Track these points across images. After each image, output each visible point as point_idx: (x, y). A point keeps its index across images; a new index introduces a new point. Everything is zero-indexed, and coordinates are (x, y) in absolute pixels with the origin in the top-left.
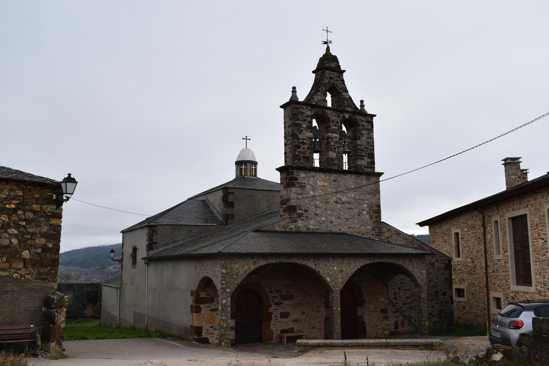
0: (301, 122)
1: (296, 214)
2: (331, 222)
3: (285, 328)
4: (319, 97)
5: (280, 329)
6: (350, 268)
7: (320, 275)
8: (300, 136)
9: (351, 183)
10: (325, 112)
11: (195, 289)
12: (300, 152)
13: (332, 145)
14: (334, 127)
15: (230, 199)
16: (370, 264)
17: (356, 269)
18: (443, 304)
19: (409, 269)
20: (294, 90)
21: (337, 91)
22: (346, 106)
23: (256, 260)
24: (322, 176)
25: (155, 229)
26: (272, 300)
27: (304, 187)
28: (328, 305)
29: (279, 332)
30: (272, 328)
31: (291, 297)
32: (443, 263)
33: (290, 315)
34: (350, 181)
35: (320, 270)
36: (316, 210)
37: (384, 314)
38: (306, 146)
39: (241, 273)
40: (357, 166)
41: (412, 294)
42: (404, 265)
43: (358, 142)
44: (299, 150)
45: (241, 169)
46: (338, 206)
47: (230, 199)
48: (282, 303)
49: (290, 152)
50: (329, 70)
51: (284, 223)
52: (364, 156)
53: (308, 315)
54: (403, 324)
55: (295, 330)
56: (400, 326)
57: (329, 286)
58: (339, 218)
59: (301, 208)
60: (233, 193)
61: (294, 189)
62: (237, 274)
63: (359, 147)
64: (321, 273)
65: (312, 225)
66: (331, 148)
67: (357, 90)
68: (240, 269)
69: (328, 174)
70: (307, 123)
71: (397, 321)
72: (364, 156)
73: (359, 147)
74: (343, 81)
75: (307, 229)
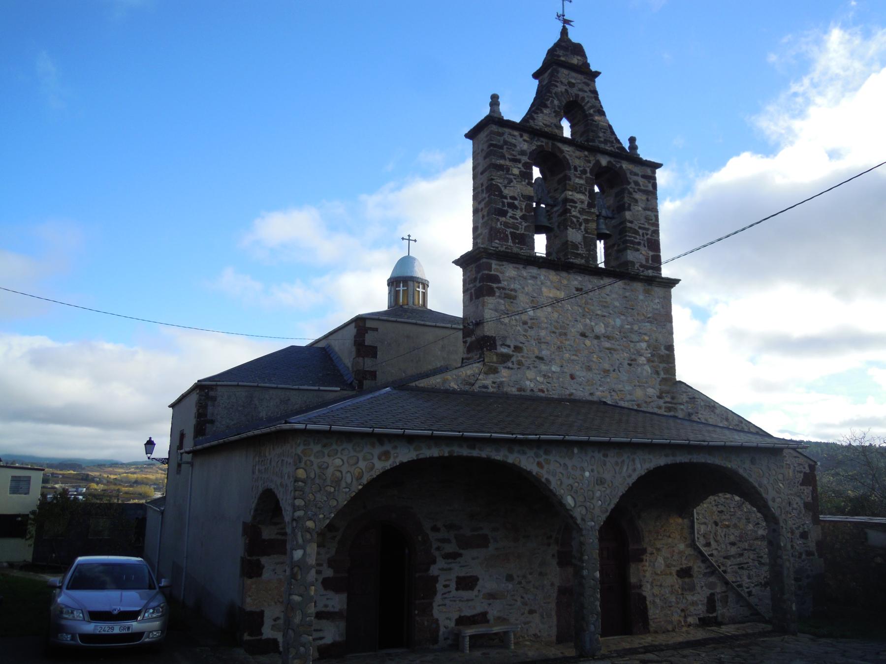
0: (508, 163)
1: (497, 354)
2: (572, 377)
3: (468, 613)
4: (546, 118)
5: (455, 616)
6: (625, 472)
7: (551, 491)
8: (506, 192)
9: (614, 296)
10: (559, 148)
11: (249, 519)
12: (506, 225)
13: (574, 216)
14: (577, 181)
15: (369, 339)
16: (667, 466)
17: (635, 477)
18: (804, 556)
19: (751, 480)
20: (495, 101)
21: (584, 111)
22: (601, 142)
23: (387, 447)
24: (553, 276)
25: (212, 393)
26: (438, 549)
27: (515, 298)
28: (567, 559)
29: (452, 624)
30: (436, 612)
31: (482, 542)
32: (801, 472)
33: (480, 583)
34: (615, 289)
35: (551, 478)
36: (541, 350)
37: (687, 580)
38: (519, 214)
39: (349, 480)
40: (627, 263)
41: (741, 537)
42: (741, 471)
43: (628, 215)
44: (504, 219)
45: (397, 292)
46: (588, 342)
47: (369, 339)
48: (460, 555)
49: (485, 224)
50: (566, 72)
51: (469, 372)
52: (639, 244)
53: (520, 583)
54: (725, 600)
55: (490, 617)
56: (718, 605)
57: (572, 517)
58: (589, 369)
59: (508, 342)
60: (376, 330)
61: (491, 301)
62: (337, 482)
63: (629, 225)
64: (554, 485)
65: (531, 380)
66: (572, 222)
67: (625, 113)
68: (344, 469)
69: (564, 274)
70: (520, 166)
71: (712, 595)
72: (639, 244)
73: (629, 225)
74: (595, 93)
75: (520, 390)
